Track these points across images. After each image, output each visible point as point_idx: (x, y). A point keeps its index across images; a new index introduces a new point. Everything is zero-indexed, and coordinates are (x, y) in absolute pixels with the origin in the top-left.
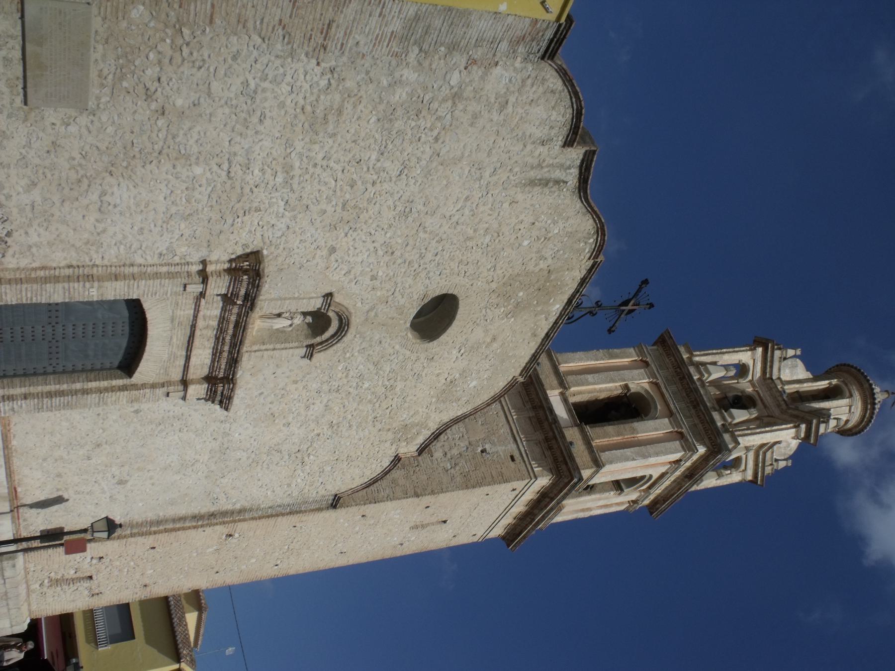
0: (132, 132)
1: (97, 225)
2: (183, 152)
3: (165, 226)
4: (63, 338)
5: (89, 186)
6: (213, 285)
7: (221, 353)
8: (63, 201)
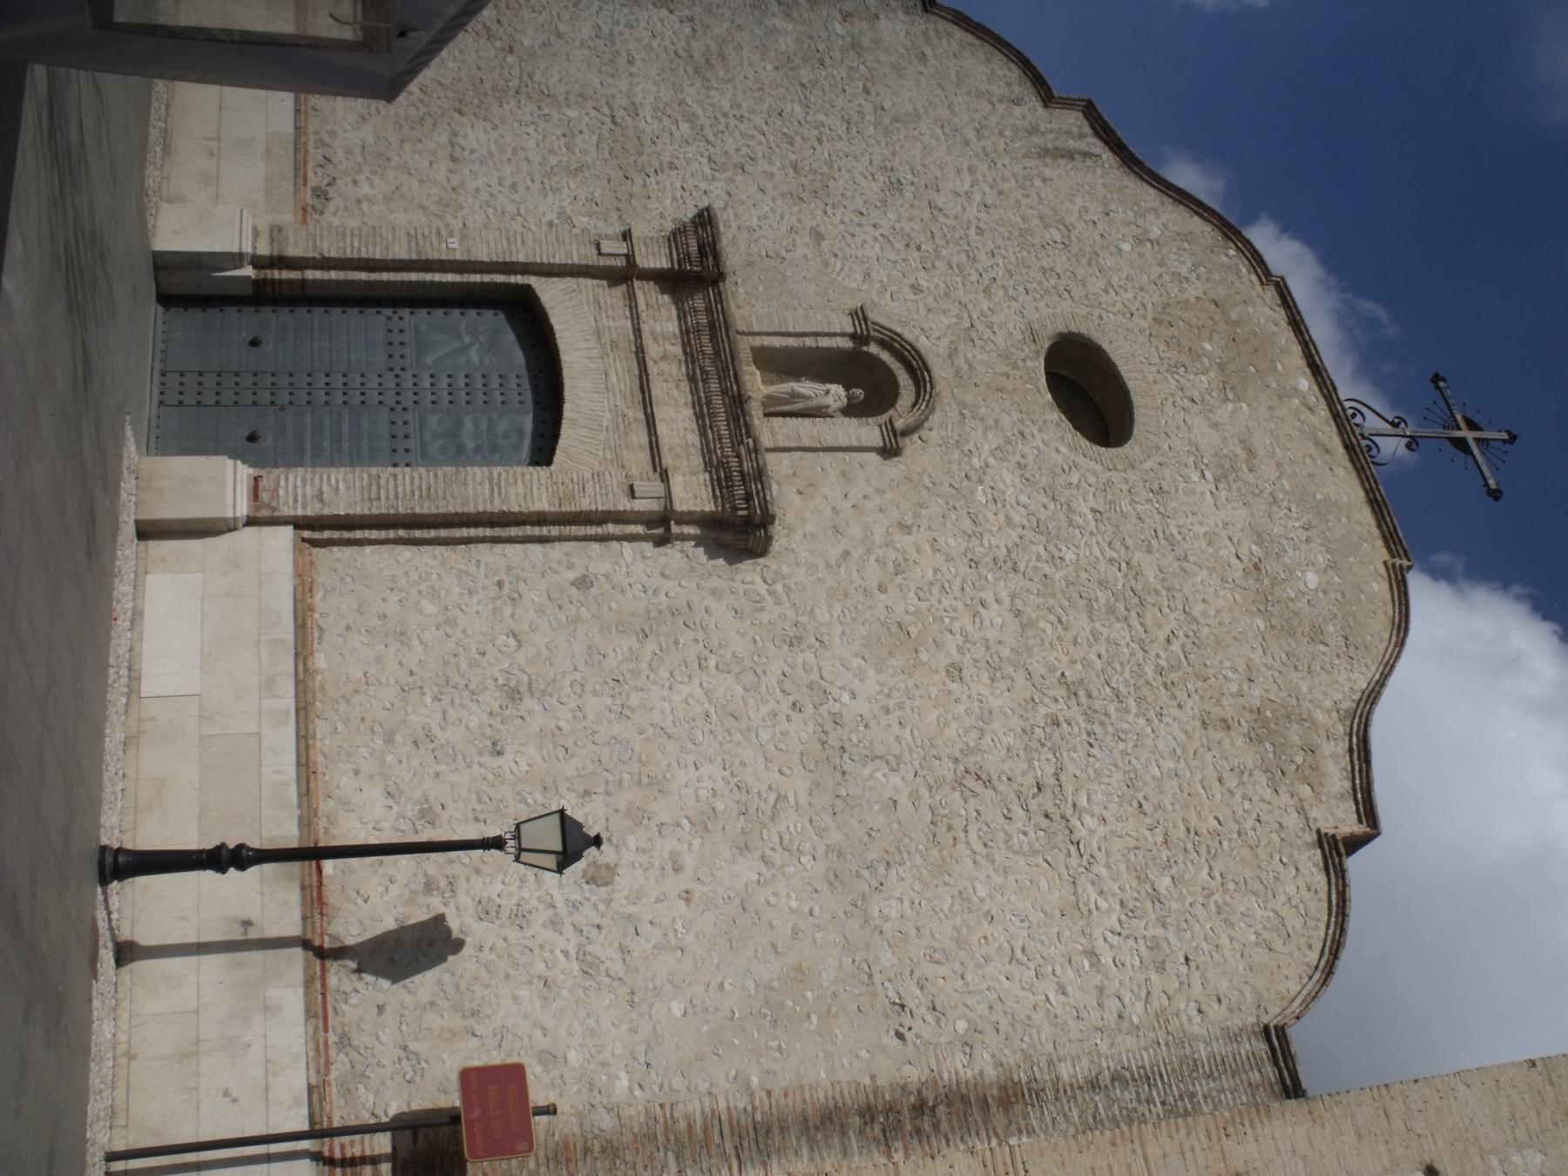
0: (479, 69)
1: (450, 176)
2: (546, 92)
3: (546, 181)
4: (416, 402)
5: (434, 125)
6: (643, 250)
7: (709, 403)
8: (402, 142)
